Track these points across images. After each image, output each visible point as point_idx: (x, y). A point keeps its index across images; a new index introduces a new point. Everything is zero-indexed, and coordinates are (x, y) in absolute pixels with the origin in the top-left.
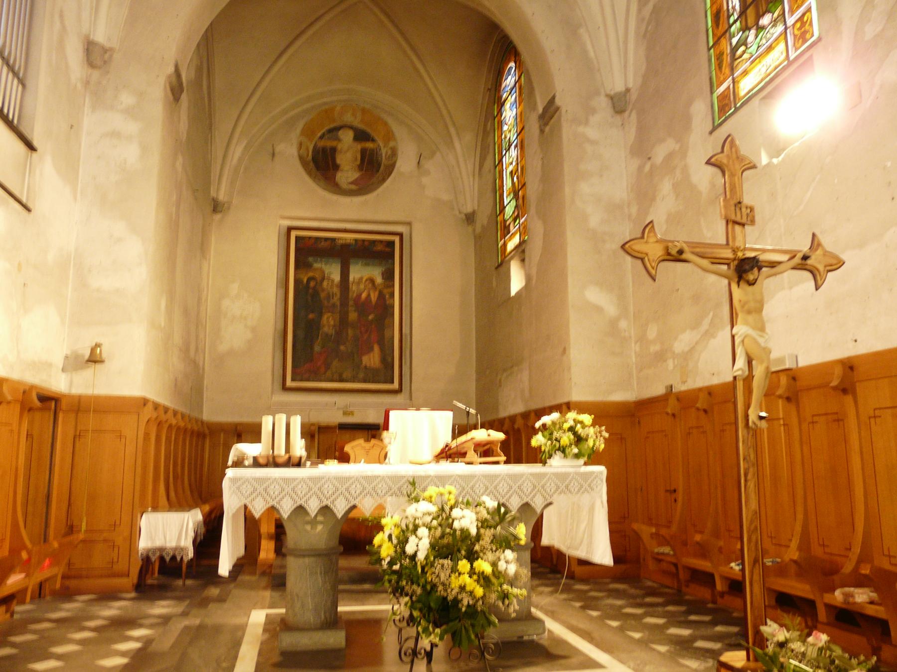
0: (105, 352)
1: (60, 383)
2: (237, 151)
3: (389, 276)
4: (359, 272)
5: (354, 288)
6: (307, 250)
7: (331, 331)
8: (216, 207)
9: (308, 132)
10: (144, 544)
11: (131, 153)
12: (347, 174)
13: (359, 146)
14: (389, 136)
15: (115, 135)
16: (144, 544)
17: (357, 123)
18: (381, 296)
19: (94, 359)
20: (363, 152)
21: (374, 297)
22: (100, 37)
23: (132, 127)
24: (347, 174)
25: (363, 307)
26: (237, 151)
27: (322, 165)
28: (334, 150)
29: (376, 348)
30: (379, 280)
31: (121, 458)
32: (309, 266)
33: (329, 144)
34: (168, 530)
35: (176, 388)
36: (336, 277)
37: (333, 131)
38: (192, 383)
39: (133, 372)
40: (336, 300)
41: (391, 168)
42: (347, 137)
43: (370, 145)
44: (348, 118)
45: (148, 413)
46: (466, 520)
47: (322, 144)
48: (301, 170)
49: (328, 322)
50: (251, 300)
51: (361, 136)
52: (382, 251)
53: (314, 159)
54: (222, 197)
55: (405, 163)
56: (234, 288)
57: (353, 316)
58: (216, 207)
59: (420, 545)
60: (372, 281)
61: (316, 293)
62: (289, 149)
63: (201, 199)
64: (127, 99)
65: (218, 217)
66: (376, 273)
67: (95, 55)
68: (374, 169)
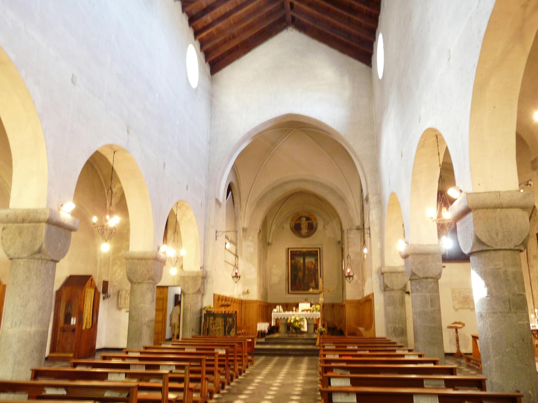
0: (249, 291)
1: (242, 297)
2: (274, 228)
3: (316, 260)
4: (308, 260)
5: (307, 265)
6: (294, 254)
7: (301, 277)
8: (269, 244)
9: (292, 220)
10: (258, 329)
11: (252, 250)
12: (304, 231)
13: (307, 222)
14: (315, 219)
15: (249, 246)
16: (258, 329)
17: (306, 215)
18: (315, 266)
19: (248, 292)
20: (309, 224)
21: (313, 267)
22: (245, 226)
23: (252, 244)
24: (304, 231)
25: (310, 270)
26: (274, 228)
27: (297, 229)
28: (300, 224)
29: (314, 282)
30: (314, 262)
31: (254, 312)
32: (294, 259)
33: (299, 222)
34: (263, 327)
35: (262, 296)
36: (302, 261)
37: (300, 218)
38: (265, 293)
39: (255, 295)
40: (302, 268)
41: (316, 228)
42: (304, 219)
43: (310, 222)
44: (304, 214)
45: (258, 303)
46: (298, 318)
47: (296, 223)
48: (291, 232)
49: (300, 274)
50: (280, 269)
51: (308, 219)
52: (314, 254)
53: (295, 227)
54: (270, 241)
55: (320, 227)
56: (274, 266)
57: (307, 272)
58: (269, 244)
59: (292, 321)
60: (312, 262)
61: (296, 266)
62: (287, 226)
63: (265, 243)
64: (250, 238)
65: (269, 247)
66: (313, 260)
67: (244, 230)
68: (312, 229)
